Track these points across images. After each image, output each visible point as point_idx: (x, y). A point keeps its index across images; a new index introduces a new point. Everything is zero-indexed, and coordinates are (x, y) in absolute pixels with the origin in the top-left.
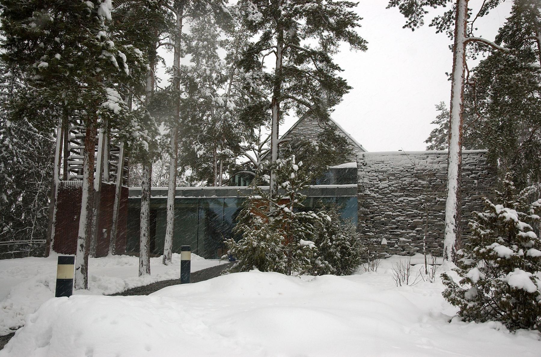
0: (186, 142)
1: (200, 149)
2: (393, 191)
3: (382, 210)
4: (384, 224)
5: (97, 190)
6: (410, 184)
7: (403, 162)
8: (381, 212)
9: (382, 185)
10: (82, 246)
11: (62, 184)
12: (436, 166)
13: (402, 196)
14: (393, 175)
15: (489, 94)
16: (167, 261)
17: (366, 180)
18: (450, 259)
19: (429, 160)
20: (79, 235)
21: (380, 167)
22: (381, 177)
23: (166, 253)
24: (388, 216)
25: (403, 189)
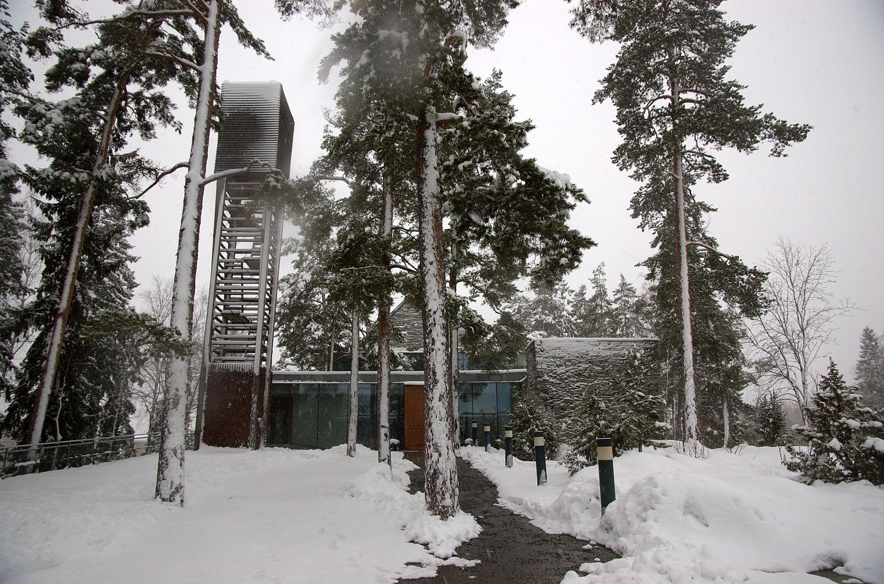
0: (299, 321)
1: (317, 329)
2: (569, 377)
3: (560, 396)
4: (563, 409)
5: (257, 374)
6: (586, 369)
7: (578, 348)
8: (559, 398)
9: (560, 370)
10: (386, 435)
11: (213, 367)
12: (608, 353)
13: (577, 382)
14: (569, 361)
15: (8, 286)
16: (353, 453)
17: (544, 366)
18: (695, 437)
19: (601, 346)
20: (382, 424)
21: (557, 353)
22: (558, 363)
23: (351, 443)
24: (566, 401)
25: (579, 375)
